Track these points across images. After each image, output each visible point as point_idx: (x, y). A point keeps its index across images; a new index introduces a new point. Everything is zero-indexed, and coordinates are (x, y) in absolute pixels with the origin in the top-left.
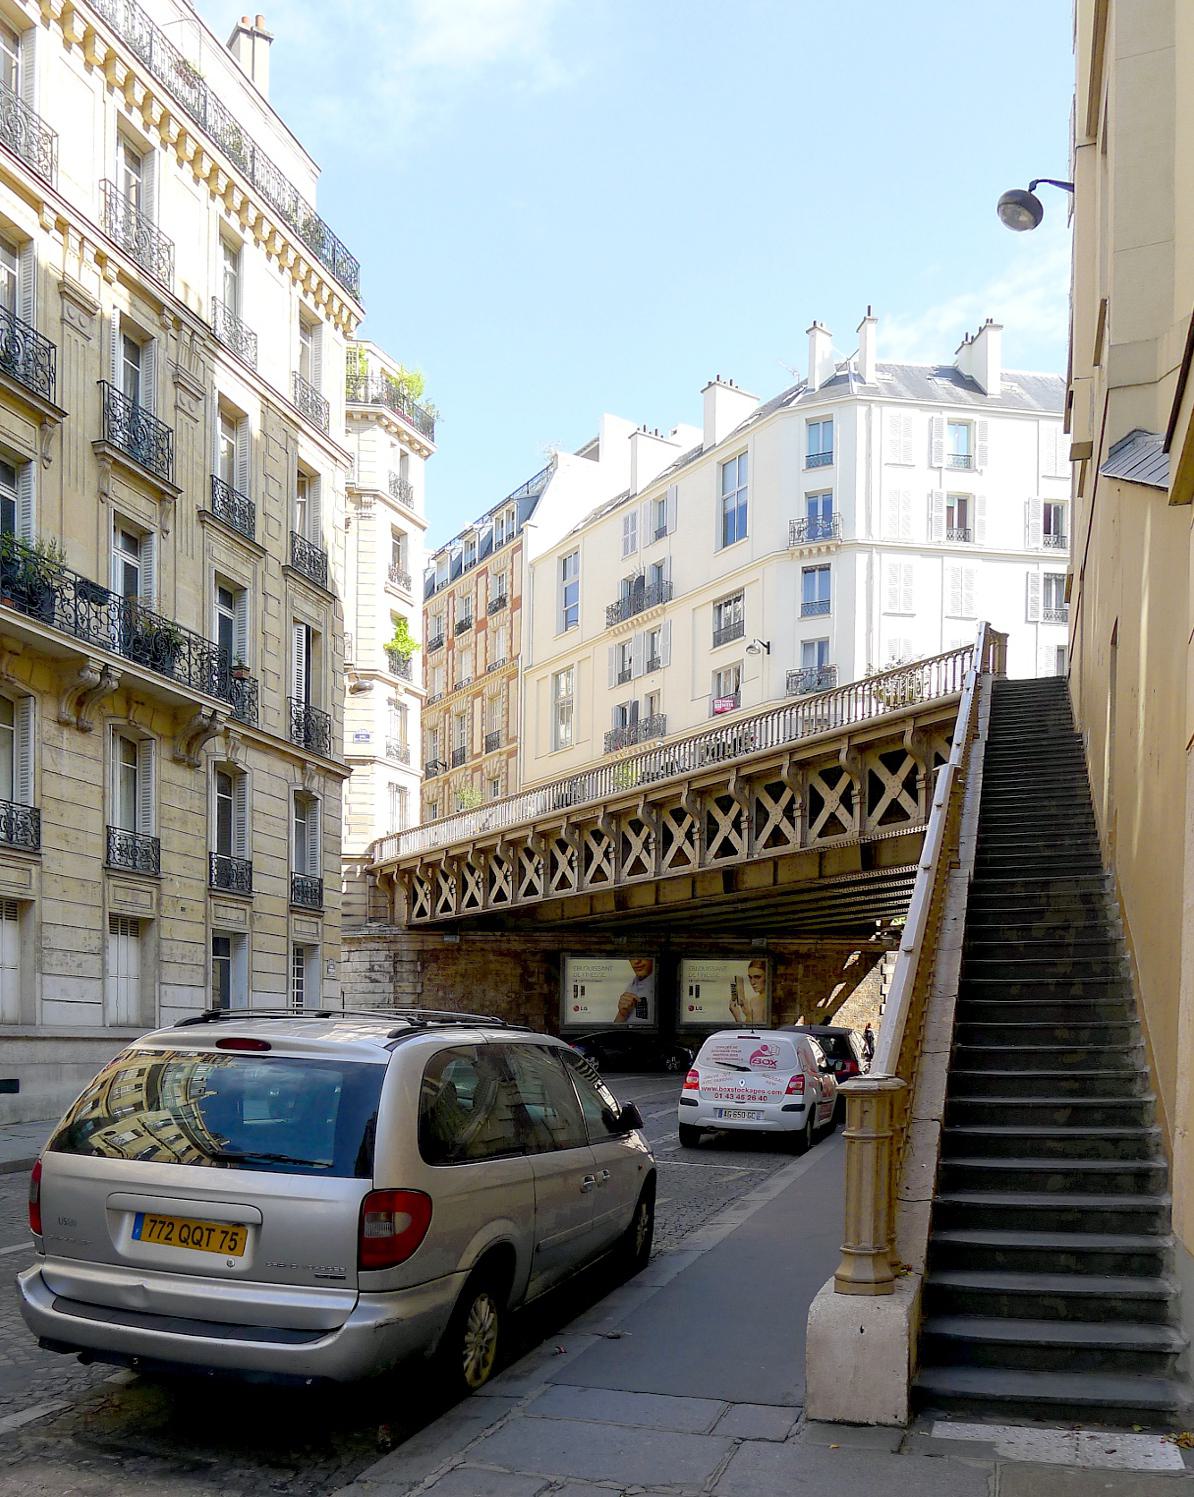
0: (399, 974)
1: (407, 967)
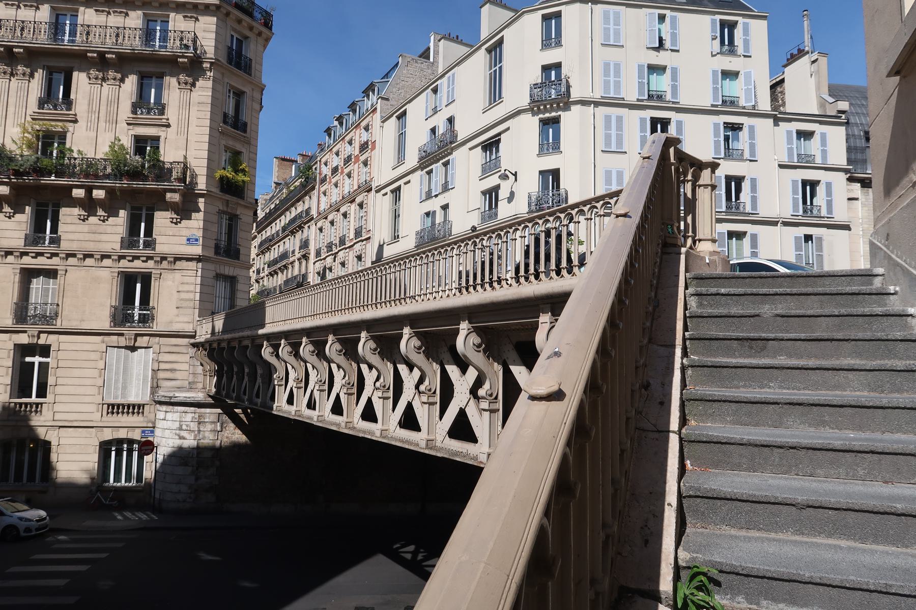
0: (201, 432)
1: (209, 427)
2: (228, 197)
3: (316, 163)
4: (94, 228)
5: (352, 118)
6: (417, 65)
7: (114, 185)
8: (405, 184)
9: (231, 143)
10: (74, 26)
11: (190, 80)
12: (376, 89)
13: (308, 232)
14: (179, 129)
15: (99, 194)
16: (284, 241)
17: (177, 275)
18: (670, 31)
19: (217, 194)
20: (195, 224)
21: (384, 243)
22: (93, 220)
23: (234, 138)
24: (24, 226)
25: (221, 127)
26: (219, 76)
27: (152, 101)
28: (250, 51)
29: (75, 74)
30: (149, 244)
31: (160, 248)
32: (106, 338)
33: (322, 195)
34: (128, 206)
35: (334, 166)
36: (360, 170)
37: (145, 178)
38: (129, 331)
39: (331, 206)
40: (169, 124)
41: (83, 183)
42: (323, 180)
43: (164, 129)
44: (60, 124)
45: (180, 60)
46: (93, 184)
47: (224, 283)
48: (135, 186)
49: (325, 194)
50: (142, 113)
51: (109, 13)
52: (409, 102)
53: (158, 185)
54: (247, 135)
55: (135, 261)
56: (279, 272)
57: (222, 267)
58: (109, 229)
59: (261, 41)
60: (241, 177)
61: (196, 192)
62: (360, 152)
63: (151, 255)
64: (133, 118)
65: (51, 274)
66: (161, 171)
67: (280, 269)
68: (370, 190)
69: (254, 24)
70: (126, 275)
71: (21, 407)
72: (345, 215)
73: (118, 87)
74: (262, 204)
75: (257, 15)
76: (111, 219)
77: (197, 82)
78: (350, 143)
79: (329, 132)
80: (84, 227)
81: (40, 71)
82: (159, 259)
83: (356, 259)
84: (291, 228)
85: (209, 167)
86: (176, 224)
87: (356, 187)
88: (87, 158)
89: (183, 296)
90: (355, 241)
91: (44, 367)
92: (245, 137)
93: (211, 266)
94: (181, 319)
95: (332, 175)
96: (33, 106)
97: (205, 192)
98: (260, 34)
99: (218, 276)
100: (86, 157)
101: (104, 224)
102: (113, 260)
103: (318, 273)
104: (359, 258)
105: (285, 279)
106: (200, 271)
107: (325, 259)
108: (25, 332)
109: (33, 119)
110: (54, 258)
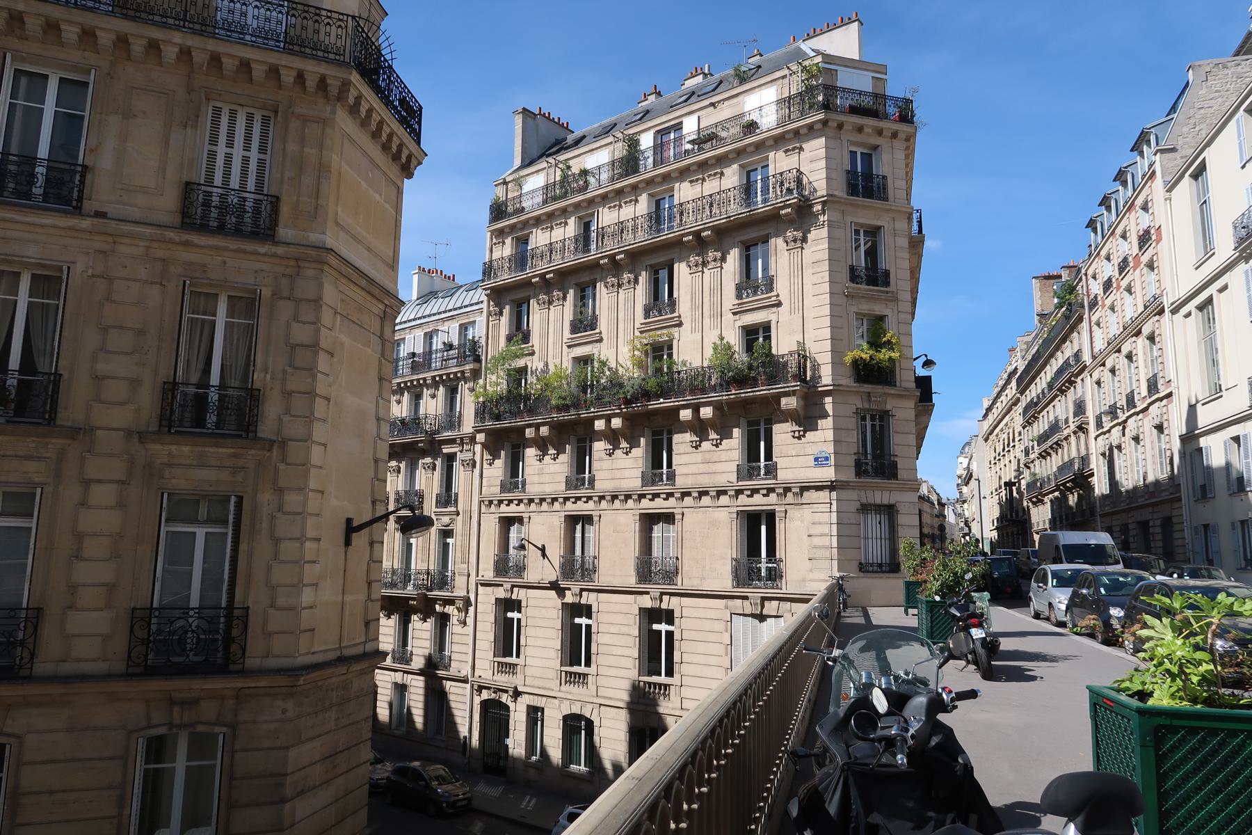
2: (867, 388)
3: (1081, 279)
4: (707, 456)
5: (1123, 194)
6: (1226, 71)
8: (1221, 290)
9: (865, 307)
10: (765, 180)
11: (799, 234)
12: (1153, 138)
13: (1083, 388)
14: (793, 305)
15: (707, 412)
16: (1052, 404)
17: (807, 511)
18: (9, 100)
19: (851, 387)
20: (823, 436)
21: (1197, 402)
22: (706, 445)
23: (871, 299)
24: (640, 463)
25: (847, 288)
26: (836, 216)
27: (760, 276)
28: (886, 164)
29: (676, 266)
30: (771, 471)
31: (784, 475)
32: (730, 602)
33: (1095, 328)
34: (743, 422)
35: (1105, 279)
36: (1143, 279)
37: (754, 382)
38: (755, 593)
39: (1109, 344)
40: (780, 301)
41: (688, 402)
42: (1094, 304)
43: (774, 309)
44: (665, 331)
45: (783, 212)
47: (878, 516)
48: (743, 395)
49: (1098, 324)
50: (747, 296)
51: (704, 180)
52: (1209, 144)
53: (769, 390)
54: (892, 288)
56: (1052, 452)
57: (870, 493)
58: (724, 455)
59: (899, 144)
60: (884, 355)
61: (820, 389)
62: (1140, 248)
63: (772, 486)
64: (739, 304)
65: (669, 518)
66: (773, 368)
67: (1051, 447)
68: (1161, 312)
69: (883, 124)
71: (650, 688)
72: (1129, 357)
74: (1021, 350)
75: (892, 110)
76: (725, 442)
77: (809, 235)
78: (1124, 237)
79: (1093, 226)
80: (697, 457)
81: (644, 273)
82: (781, 491)
83: (1155, 431)
84: (1057, 385)
85: (834, 351)
86: (799, 438)
87: (1141, 309)
89: (817, 541)
90: (1149, 401)
91: (670, 635)
92: (887, 292)
93: (852, 495)
94: (816, 575)
95: (1105, 293)
96: (640, 318)
97: (831, 388)
98: (895, 135)
99: (865, 508)
103: (1103, 455)
104: (1160, 428)
105: (1061, 464)
106: (834, 503)
107: (1109, 431)
108: (647, 593)
109: (641, 332)
110: (670, 499)
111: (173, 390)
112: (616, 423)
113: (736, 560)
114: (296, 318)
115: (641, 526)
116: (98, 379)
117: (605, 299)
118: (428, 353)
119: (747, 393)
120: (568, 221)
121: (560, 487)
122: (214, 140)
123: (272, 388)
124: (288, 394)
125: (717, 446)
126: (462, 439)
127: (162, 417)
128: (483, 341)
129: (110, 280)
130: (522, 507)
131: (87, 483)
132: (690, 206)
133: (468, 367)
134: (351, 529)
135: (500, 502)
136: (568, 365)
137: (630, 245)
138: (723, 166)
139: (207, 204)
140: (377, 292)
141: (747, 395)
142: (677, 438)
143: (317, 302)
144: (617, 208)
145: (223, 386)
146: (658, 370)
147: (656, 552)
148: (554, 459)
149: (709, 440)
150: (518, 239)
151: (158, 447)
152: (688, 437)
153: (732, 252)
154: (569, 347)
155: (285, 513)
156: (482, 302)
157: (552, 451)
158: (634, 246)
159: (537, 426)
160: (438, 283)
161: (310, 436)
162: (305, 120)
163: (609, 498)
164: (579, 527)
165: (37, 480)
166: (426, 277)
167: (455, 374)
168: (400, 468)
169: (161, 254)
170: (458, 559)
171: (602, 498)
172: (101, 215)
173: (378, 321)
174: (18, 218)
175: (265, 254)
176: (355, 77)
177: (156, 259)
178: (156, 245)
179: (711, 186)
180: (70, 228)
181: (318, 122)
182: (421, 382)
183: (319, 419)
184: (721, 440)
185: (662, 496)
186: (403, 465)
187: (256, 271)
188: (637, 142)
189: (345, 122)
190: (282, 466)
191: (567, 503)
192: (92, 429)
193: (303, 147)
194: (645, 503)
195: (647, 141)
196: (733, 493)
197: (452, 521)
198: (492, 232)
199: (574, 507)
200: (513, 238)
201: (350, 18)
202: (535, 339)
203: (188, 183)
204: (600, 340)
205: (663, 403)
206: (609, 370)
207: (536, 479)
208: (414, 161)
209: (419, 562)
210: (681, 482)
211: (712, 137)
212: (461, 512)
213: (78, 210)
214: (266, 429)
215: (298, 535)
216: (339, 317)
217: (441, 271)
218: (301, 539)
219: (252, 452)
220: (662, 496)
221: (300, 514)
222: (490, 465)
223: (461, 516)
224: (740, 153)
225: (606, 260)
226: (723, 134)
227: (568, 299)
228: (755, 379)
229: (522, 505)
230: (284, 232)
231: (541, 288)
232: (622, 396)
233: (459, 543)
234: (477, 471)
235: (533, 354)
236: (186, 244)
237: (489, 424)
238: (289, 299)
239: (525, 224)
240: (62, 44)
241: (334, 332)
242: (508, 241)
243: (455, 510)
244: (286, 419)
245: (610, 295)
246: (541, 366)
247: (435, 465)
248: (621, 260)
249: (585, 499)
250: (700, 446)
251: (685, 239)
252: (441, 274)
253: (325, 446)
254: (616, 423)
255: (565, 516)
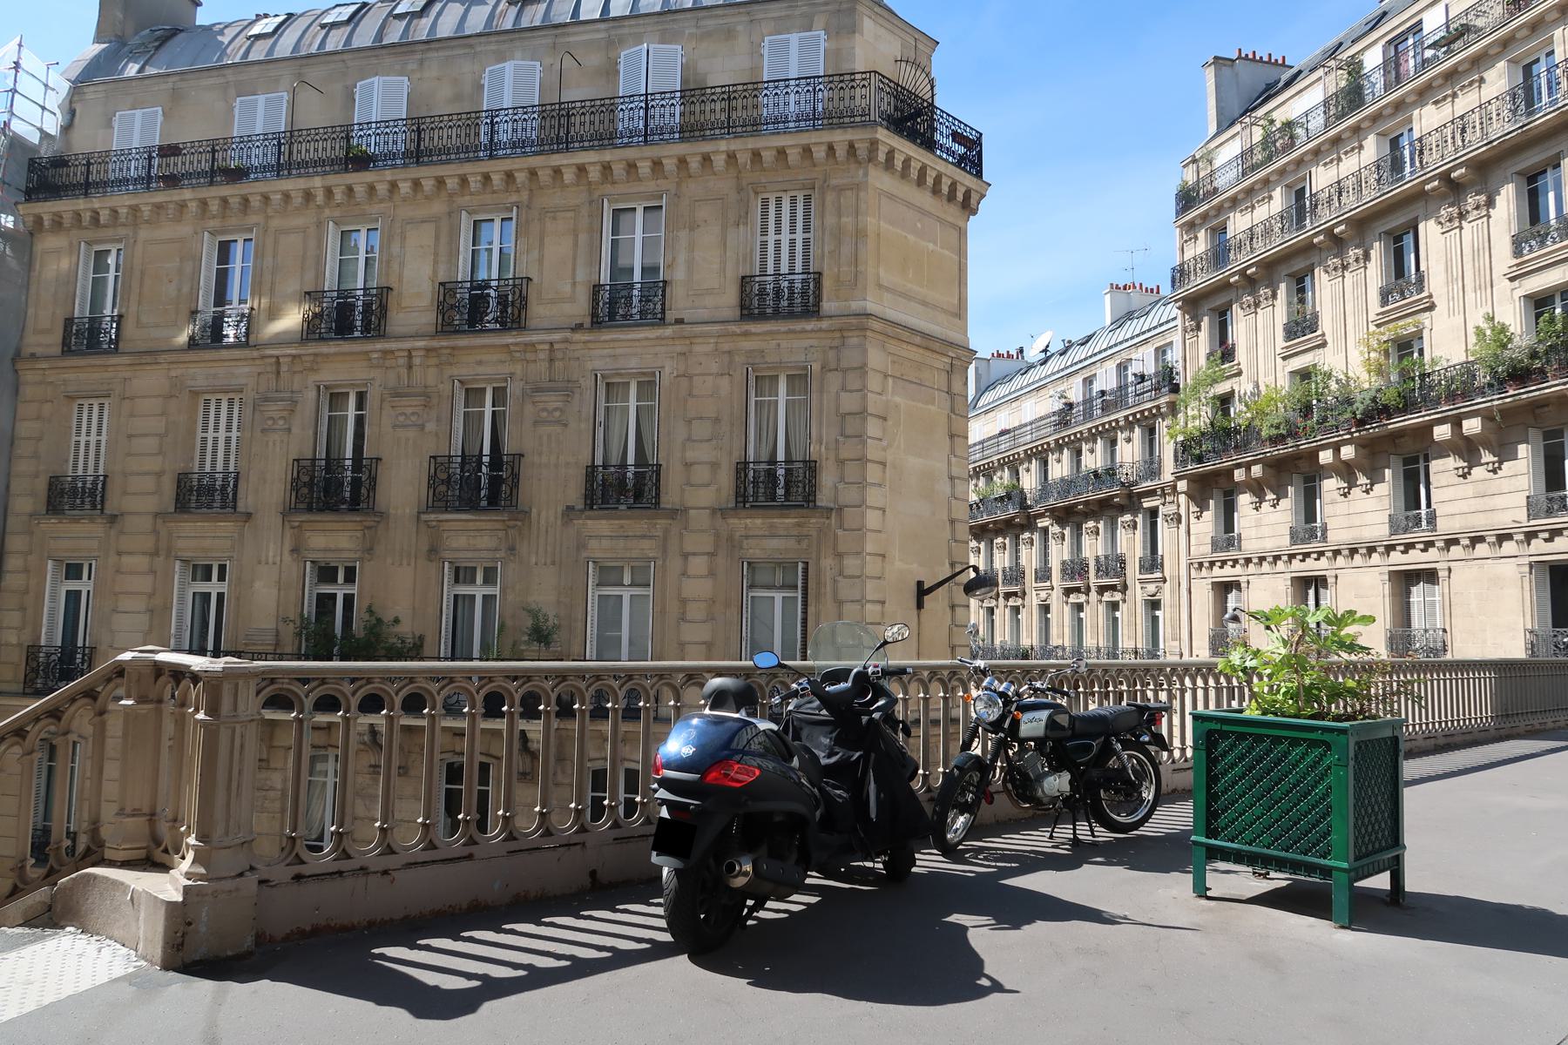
7: (1489, 404)
15: (1472, 426)
22: (1478, 472)
24: (1386, 503)
29: (1421, 227)
31: (1445, 526)
40: (1433, 303)
44: (1409, 320)
46: (1458, 411)
48: (1524, 396)
50: (1531, 251)
51: (1454, 95)
55: (1556, 539)
58: (1506, 485)
64: (1517, 265)
65: (1430, 576)
70: (1550, 567)
73: (1457, 230)
76: (1506, 465)
80: (1467, 489)
88: (1454, 366)
96: (1375, 307)
100: (1450, 364)
101: (1497, 476)
102: (1517, 541)
110: (1430, 549)
111: (745, 468)
112: (1348, 452)
113: (1531, 632)
114: (844, 389)
115: (1393, 588)
116: (688, 465)
117: (1326, 289)
118: (1122, 388)
119: (1532, 392)
120: (1273, 194)
121: (1283, 542)
122: (764, 232)
123: (827, 459)
124: (841, 462)
125: (1494, 471)
126: (1163, 489)
127: (737, 495)
128: (1179, 367)
129: (690, 377)
130: (1238, 569)
131: (685, 556)
132: (1433, 139)
133: (1163, 400)
134: (922, 592)
135: (1212, 564)
136: (1284, 382)
137: (1351, 210)
138: (1482, 69)
139: (762, 293)
140: (937, 346)
141: (1531, 395)
142: (1435, 465)
143: (862, 369)
144: (1335, 162)
145: (788, 461)
146: (1405, 376)
147: (1417, 622)
148: (1274, 506)
149: (1482, 465)
150: (1213, 230)
151: (736, 521)
152: (1452, 462)
153: (1503, 191)
154: (1284, 358)
155: (845, 577)
156: (1175, 318)
157: (1270, 496)
158: (1358, 210)
159: (1248, 466)
160: (1137, 299)
161: (864, 501)
162: (840, 190)
163: (1346, 552)
164: (1311, 592)
165: (651, 555)
166: (1121, 295)
167: (1150, 410)
168: (1098, 528)
169: (726, 347)
170: (1168, 635)
171: (1337, 553)
172: (680, 321)
173: (944, 376)
174: (622, 337)
175: (812, 331)
176: (883, 134)
177: (724, 352)
178: (721, 340)
179: (1466, 101)
180: (657, 338)
181: (852, 189)
182: (1114, 424)
183: (874, 484)
184: (1501, 463)
185: (1418, 546)
186: (1101, 526)
187: (806, 349)
188: (1361, 63)
189: (879, 180)
190: (840, 532)
191: (1294, 561)
192: (686, 510)
193: (840, 216)
194: (1396, 557)
195: (1373, 59)
196: (1521, 537)
197: (1159, 589)
198: (1181, 226)
199: (1303, 566)
200: (1206, 230)
201: (873, 74)
202: (1241, 355)
203: (743, 278)
204: (1324, 345)
205: (1413, 420)
206: (1337, 383)
207: (1253, 533)
208: (974, 197)
209: (1125, 638)
210: (1445, 526)
211: (1465, 30)
212: (1168, 579)
213: (662, 321)
214: (824, 498)
215: (859, 598)
216: (890, 380)
217: (1141, 284)
218: (862, 601)
219: (813, 520)
220: (1418, 546)
221: (859, 577)
222: (1198, 518)
223: (1168, 583)
224: (1506, 43)
225: (1322, 237)
226: (1480, 22)
227: (1279, 296)
228: (1542, 371)
229: (1238, 566)
230: (827, 306)
231: (1244, 288)
232: (1348, 415)
233: (1168, 616)
234: (1183, 526)
235: (1239, 374)
236: (746, 334)
237: (1192, 468)
238: (837, 370)
239: (1220, 209)
240: (640, 180)
241: (882, 393)
242: (1202, 234)
243: (1161, 575)
244: (841, 486)
245: (1333, 282)
246: (1249, 388)
247: (1135, 523)
248: (1341, 233)
249: (1315, 556)
250: (1470, 474)
251: (1428, 187)
252: (1141, 288)
253: (883, 510)
254: (1348, 452)
255: (1292, 578)
